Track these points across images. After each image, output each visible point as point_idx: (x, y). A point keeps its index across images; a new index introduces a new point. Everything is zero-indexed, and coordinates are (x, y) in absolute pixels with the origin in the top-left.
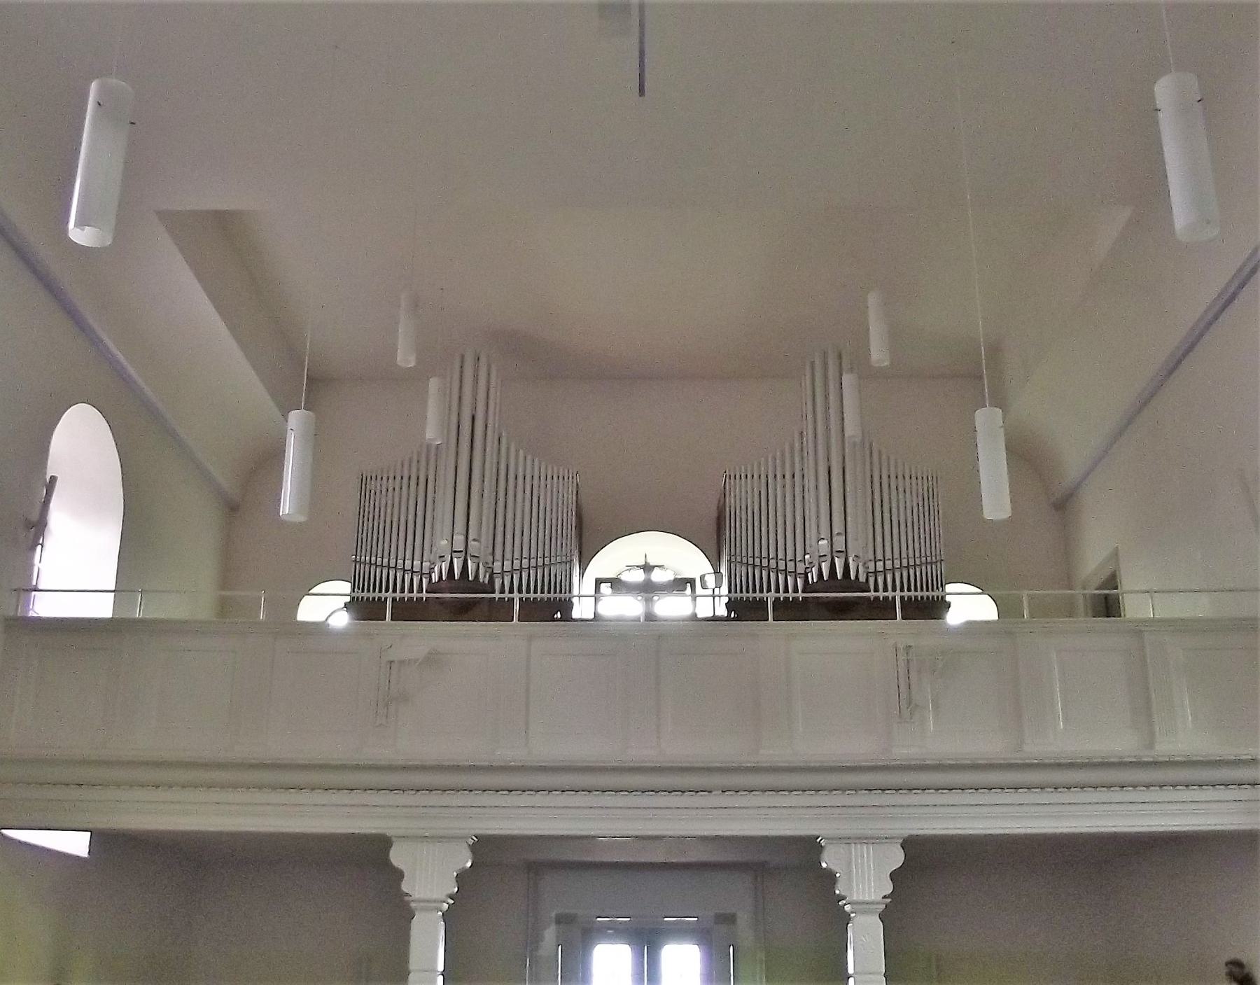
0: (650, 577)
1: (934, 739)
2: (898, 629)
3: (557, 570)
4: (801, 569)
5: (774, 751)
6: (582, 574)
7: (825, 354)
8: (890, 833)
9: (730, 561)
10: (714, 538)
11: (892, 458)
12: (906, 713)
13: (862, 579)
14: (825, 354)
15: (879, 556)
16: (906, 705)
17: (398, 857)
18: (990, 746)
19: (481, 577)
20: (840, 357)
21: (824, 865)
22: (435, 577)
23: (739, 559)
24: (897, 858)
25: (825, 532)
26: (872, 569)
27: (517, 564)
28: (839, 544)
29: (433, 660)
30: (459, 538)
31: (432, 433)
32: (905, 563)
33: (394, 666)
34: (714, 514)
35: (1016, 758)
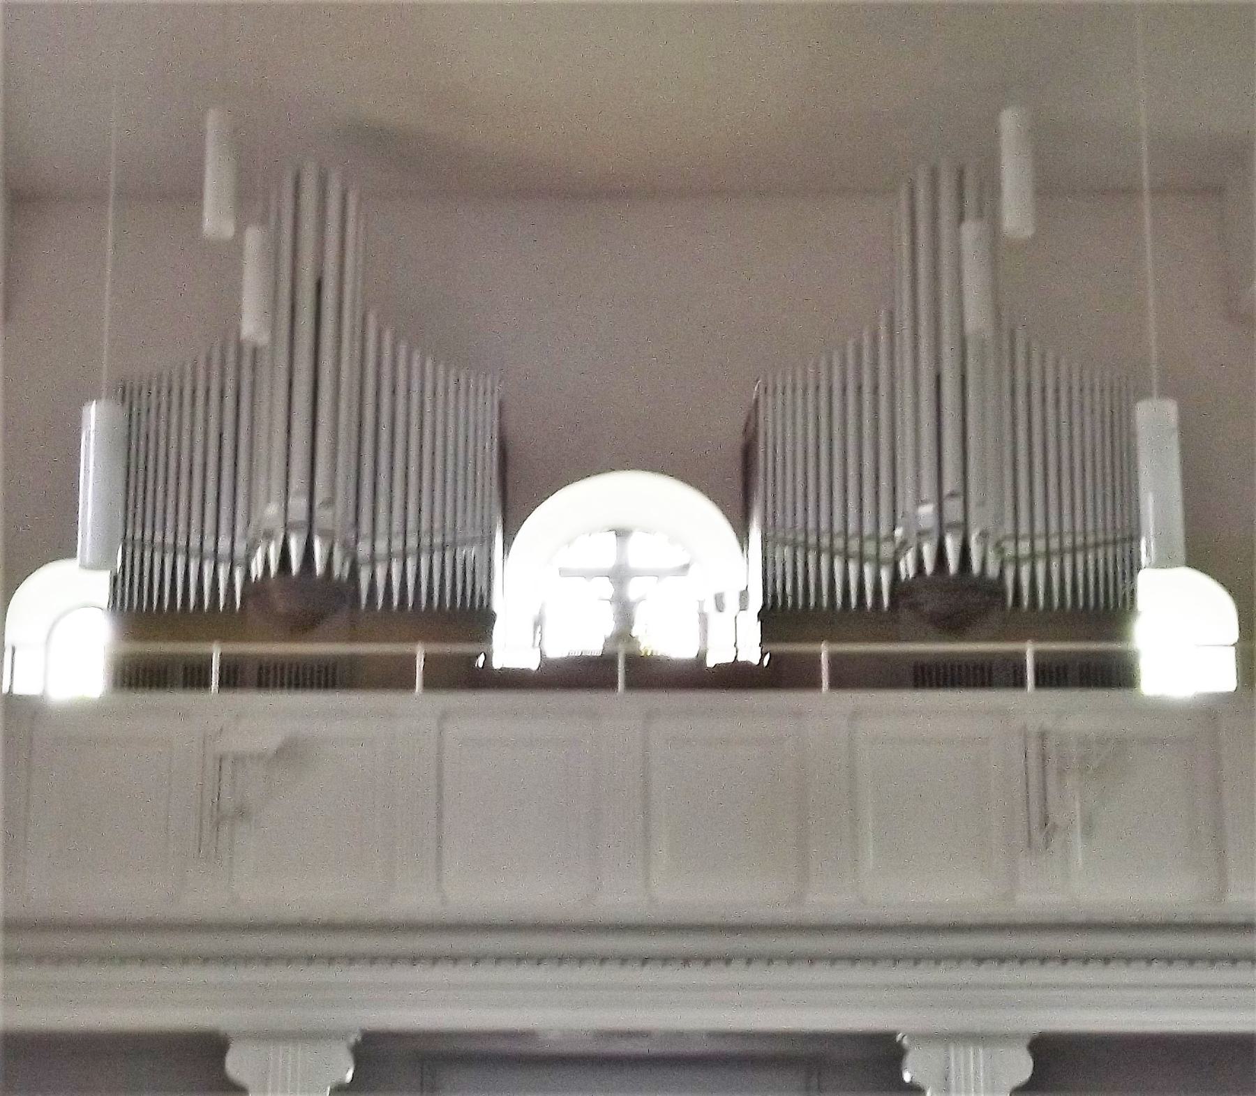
0: (629, 563)
1: (1084, 881)
2: (1032, 705)
3: (471, 552)
4: (887, 550)
5: (827, 899)
6: (507, 544)
7: (934, 174)
8: (1009, 1028)
9: (764, 540)
10: (738, 488)
11: (1050, 355)
12: (1038, 838)
13: (993, 570)
14: (934, 174)
15: (1024, 529)
16: (1043, 830)
17: (237, 1065)
18: (1170, 891)
19: (336, 573)
20: (961, 174)
21: (907, 1077)
22: (257, 569)
23: (780, 534)
24: (1021, 1067)
25: (928, 489)
26: (1010, 552)
27: (397, 545)
28: (953, 510)
29: (291, 754)
30: (298, 505)
31: (251, 327)
32: (1068, 542)
33: (227, 766)
34: (738, 441)
35: (1210, 913)
